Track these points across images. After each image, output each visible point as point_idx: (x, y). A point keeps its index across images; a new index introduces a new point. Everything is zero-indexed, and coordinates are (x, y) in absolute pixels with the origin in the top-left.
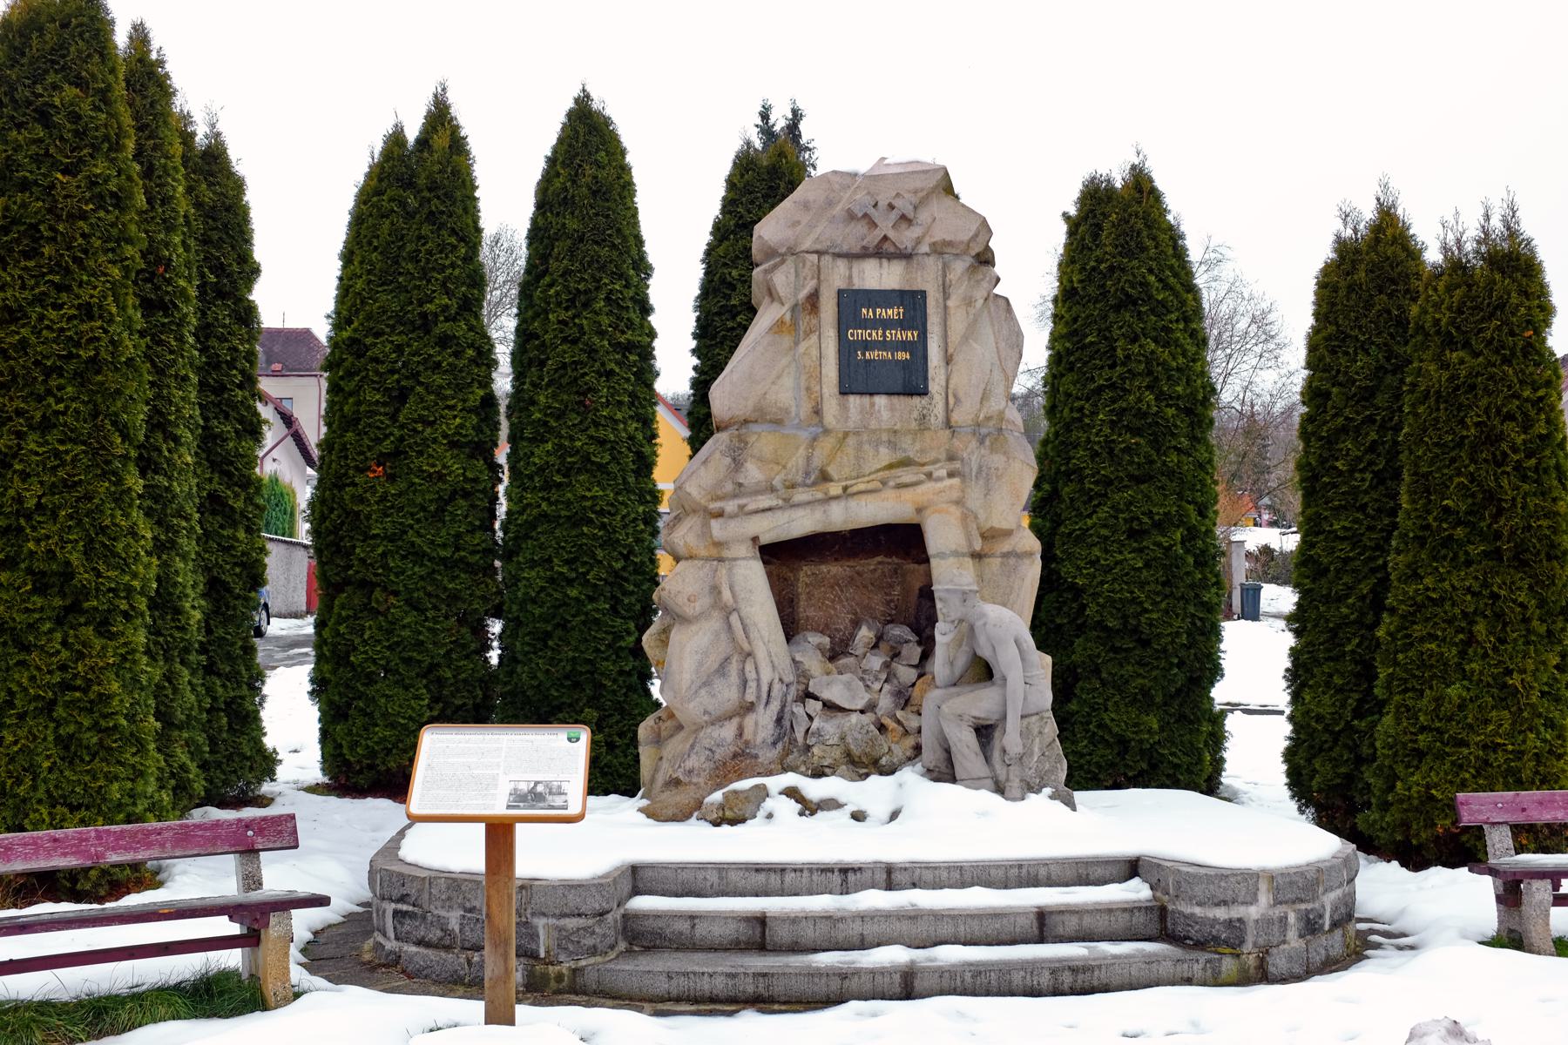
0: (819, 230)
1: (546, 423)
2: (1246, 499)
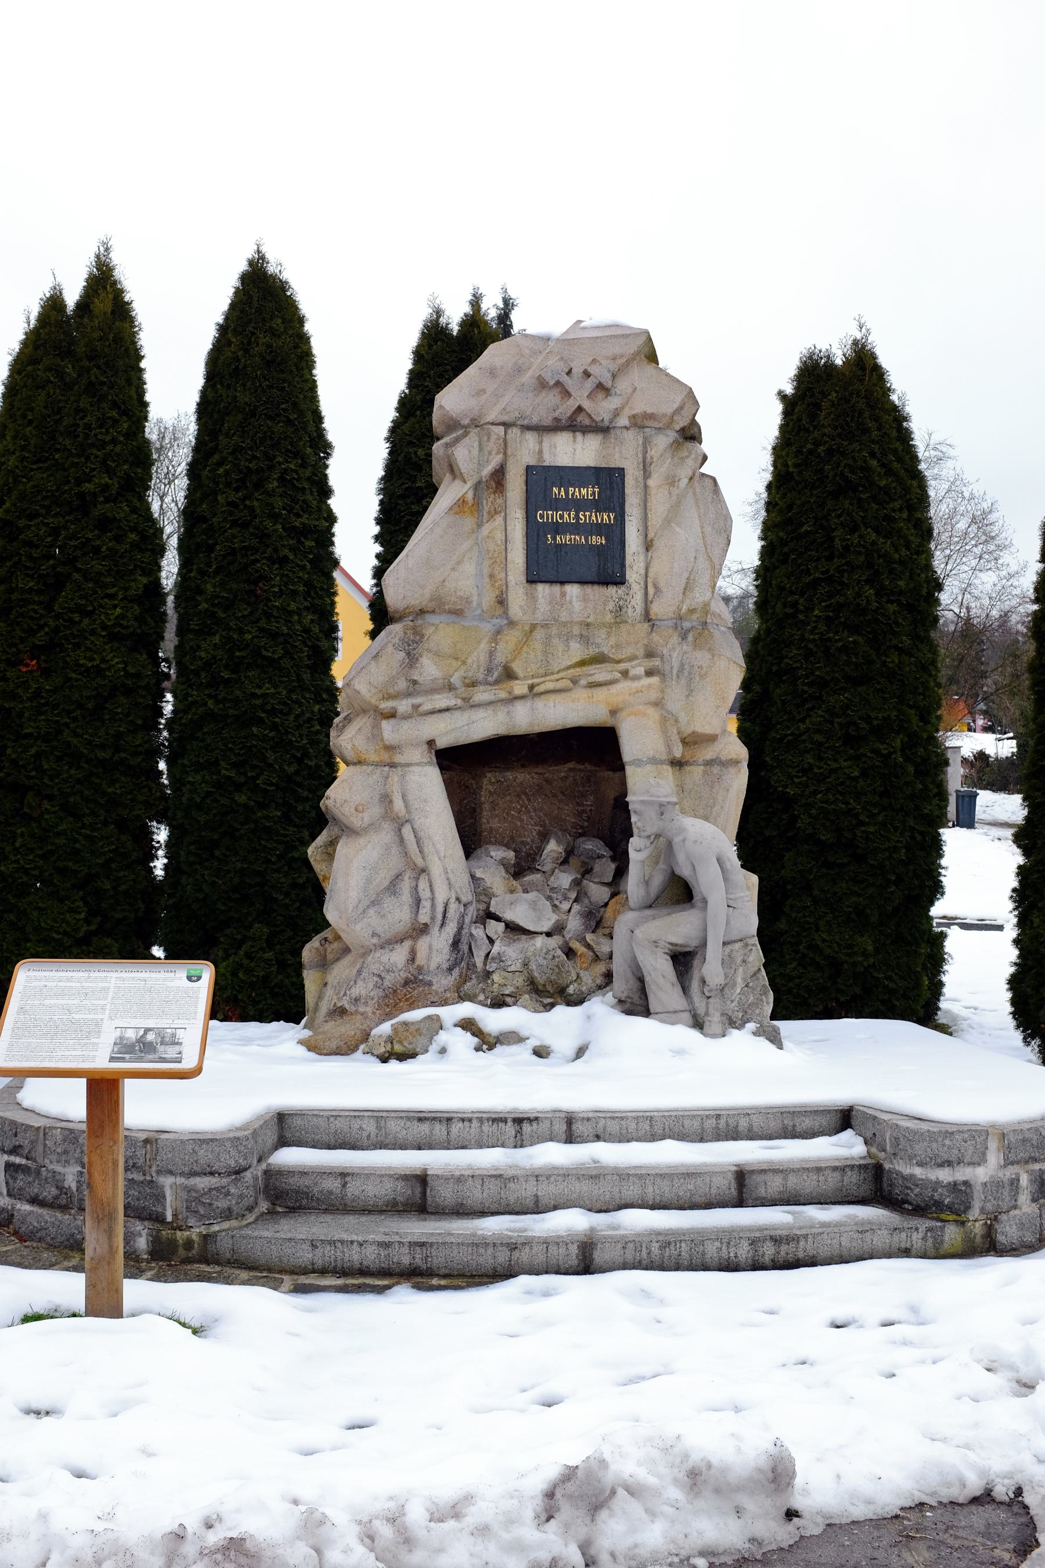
0: (506, 399)
1: (213, 615)
2: (962, 705)
